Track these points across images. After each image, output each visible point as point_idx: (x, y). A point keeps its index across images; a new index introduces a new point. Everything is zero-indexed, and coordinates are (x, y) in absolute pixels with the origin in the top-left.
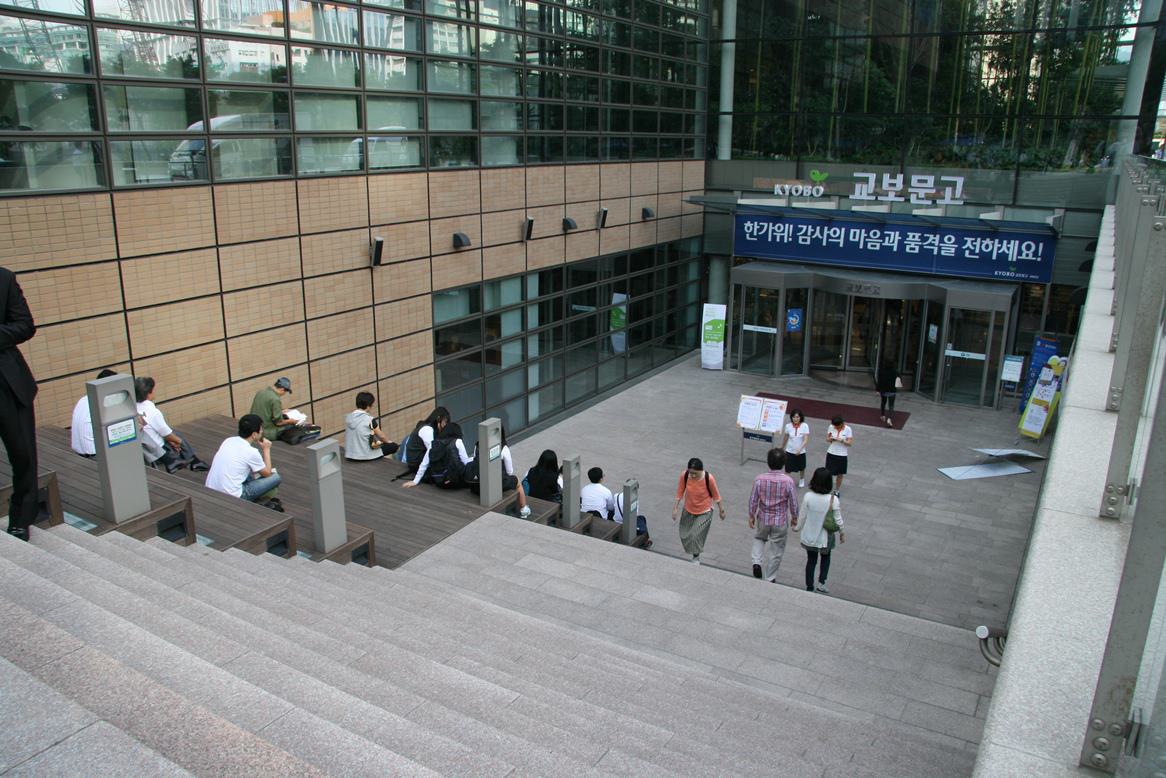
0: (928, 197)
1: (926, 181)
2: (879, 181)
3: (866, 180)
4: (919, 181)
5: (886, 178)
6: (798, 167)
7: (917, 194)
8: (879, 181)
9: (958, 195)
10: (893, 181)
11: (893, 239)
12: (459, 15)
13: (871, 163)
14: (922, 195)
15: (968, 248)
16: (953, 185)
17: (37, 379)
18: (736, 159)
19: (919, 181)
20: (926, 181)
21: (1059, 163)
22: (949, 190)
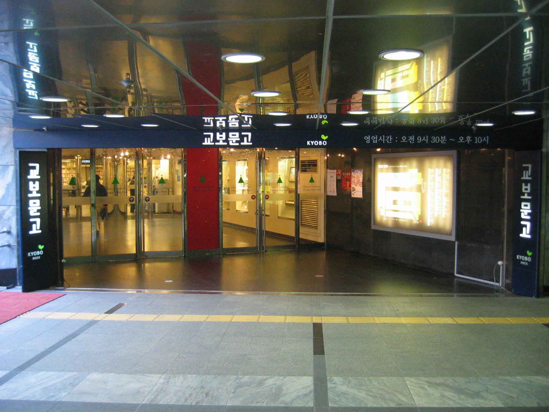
0: (237, 142)
1: (235, 135)
2: (215, 136)
3: (209, 136)
4: (233, 135)
5: (442, 137)
6: (296, 113)
7: (232, 141)
8: (215, 136)
9: (249, 140)
10: (221, 136)
11: (420, 139)
12: (75, 162)
13: (542, 407)
14: (234, 141)
15: (410, 140)
16: (247, 136)
17: (300, 149)
18: (233, 202)
19: (233, 135)
20: (235, 135)
21: (350, 386)
22: (245, 138)
